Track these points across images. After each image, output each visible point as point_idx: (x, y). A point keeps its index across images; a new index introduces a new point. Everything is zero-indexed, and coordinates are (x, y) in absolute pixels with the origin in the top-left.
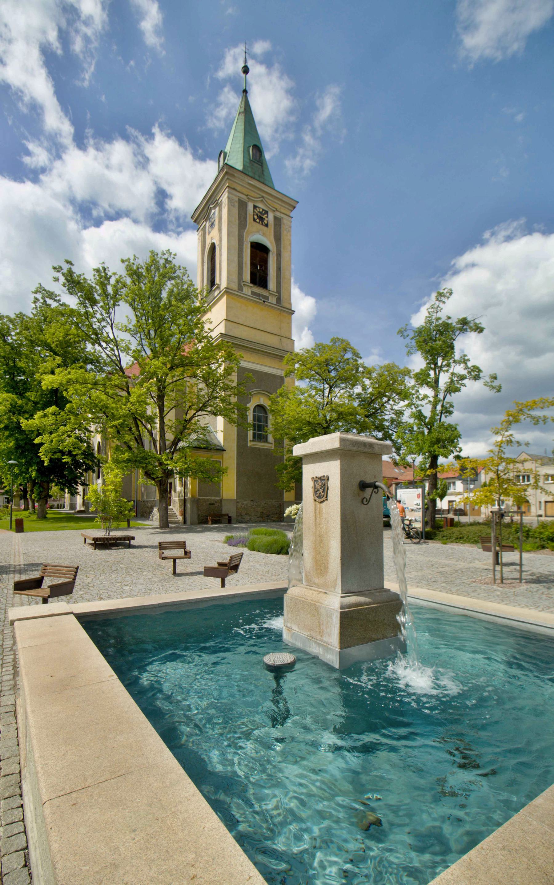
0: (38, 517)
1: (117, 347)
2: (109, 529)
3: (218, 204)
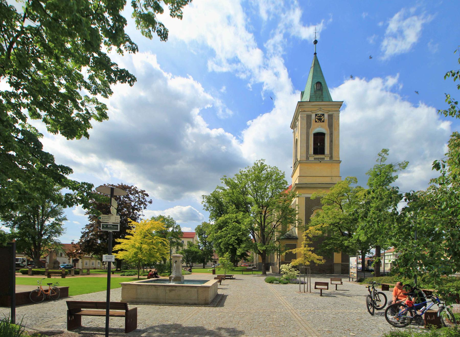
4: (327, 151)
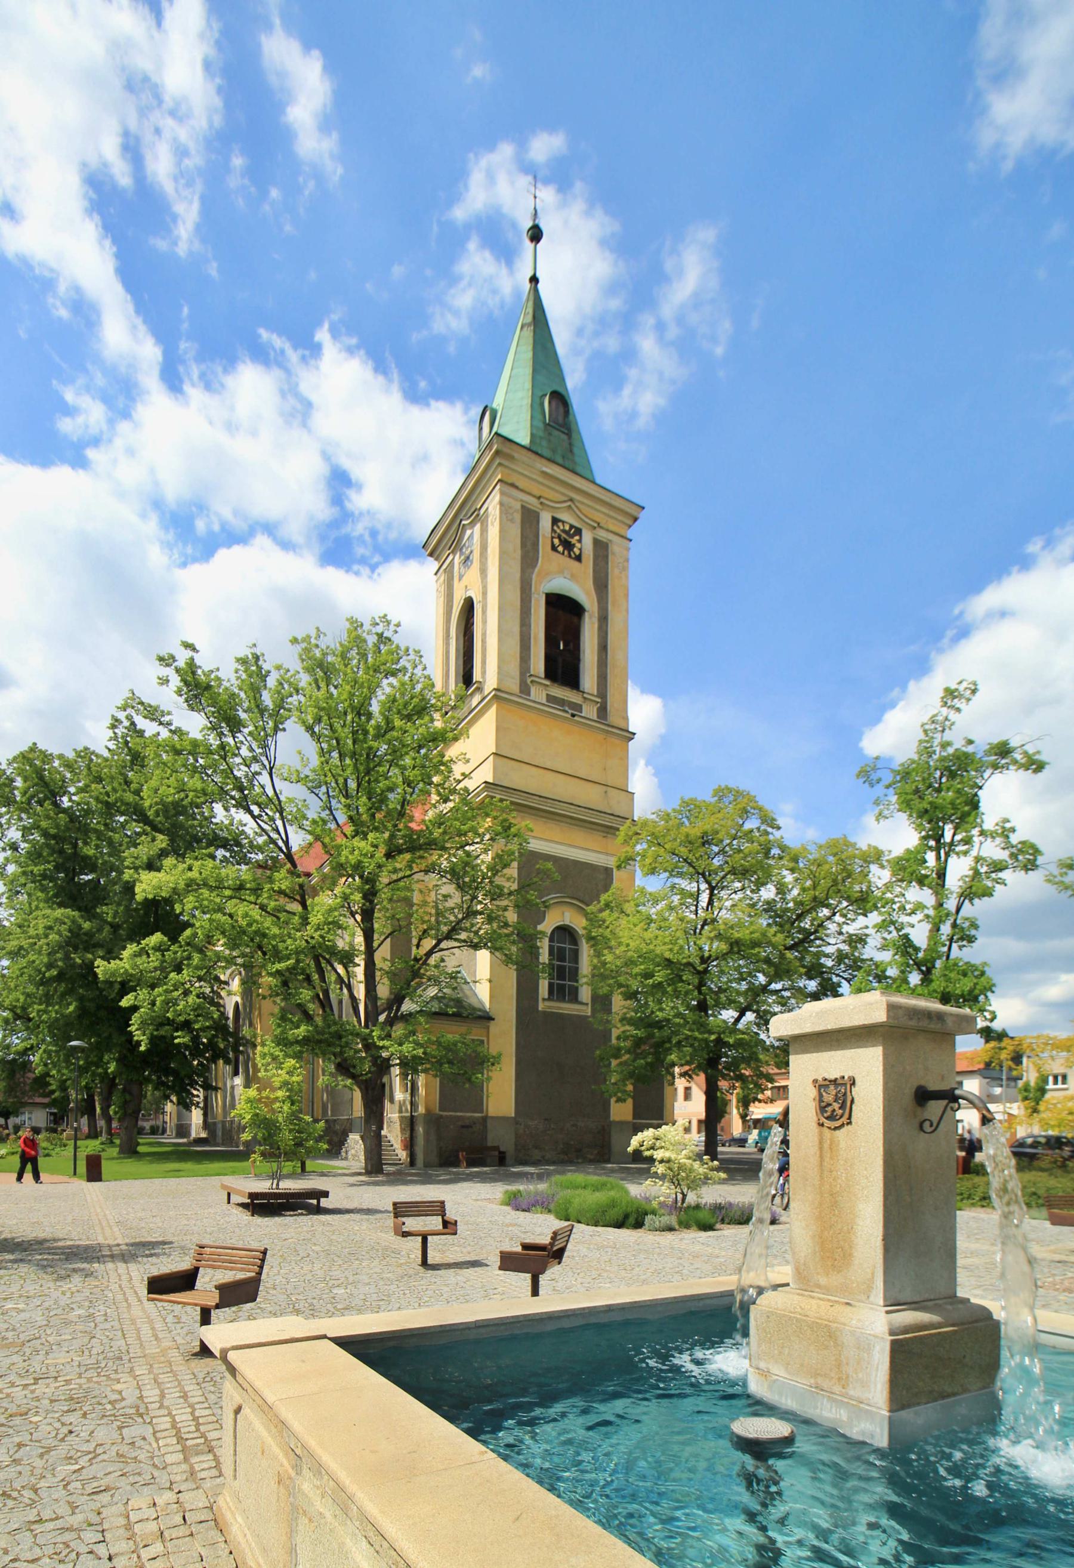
0: (120, 1152)
1: (281, 814)
2: (276, 1176)
3: (478, 517)
4: (589, 679)
